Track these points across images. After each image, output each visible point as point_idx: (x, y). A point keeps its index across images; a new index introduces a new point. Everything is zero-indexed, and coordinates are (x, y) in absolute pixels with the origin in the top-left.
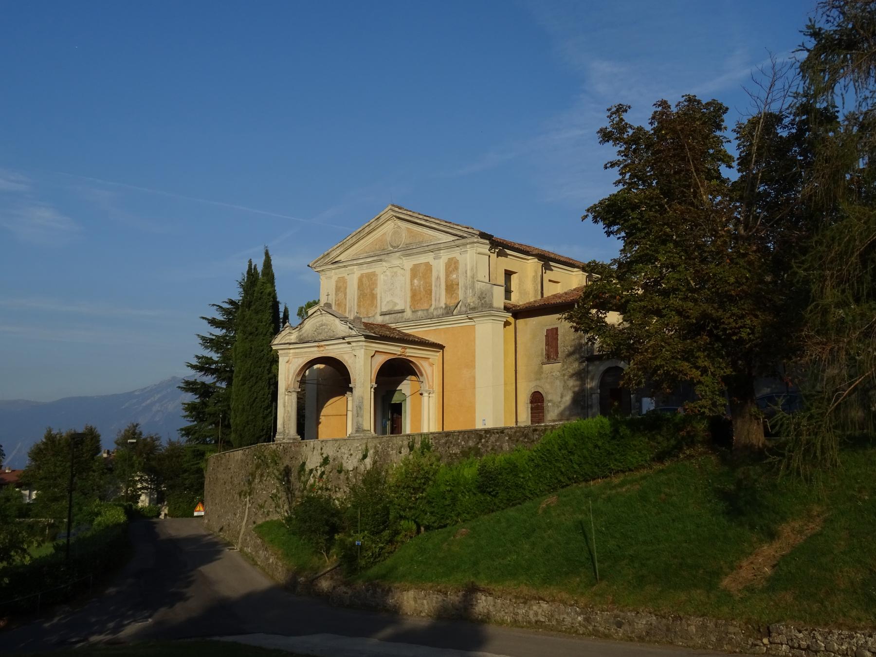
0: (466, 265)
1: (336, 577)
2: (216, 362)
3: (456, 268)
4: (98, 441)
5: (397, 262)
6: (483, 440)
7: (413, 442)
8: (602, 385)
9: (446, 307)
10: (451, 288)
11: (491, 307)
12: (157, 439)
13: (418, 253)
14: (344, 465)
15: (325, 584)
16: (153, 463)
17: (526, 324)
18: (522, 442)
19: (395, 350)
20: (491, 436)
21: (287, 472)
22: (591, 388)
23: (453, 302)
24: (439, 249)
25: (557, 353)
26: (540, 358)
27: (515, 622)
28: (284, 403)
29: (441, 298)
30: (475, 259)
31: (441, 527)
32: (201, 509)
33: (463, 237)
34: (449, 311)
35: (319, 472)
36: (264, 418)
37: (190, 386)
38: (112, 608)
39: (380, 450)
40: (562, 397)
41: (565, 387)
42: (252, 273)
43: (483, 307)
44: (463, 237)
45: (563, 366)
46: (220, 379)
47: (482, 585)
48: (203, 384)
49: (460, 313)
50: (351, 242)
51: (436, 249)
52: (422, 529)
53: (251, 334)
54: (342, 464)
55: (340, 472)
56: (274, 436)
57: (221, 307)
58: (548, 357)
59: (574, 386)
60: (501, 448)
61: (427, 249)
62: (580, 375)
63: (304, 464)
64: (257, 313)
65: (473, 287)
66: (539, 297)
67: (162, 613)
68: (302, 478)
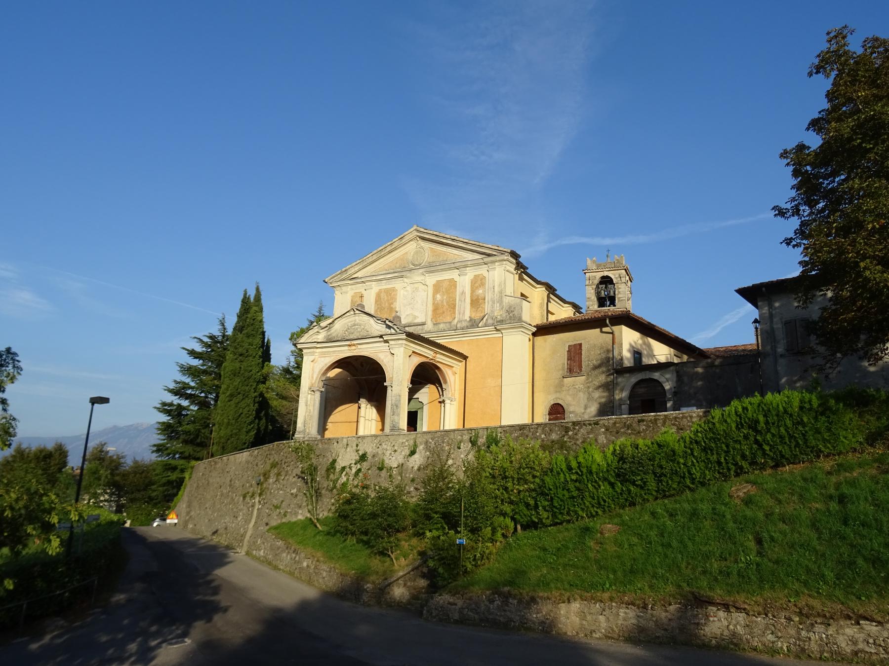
0: (494, 281)
1: (409, 584)
2: (192, 388)
3: (483, 284)
4: (66, 456)
5: (420, 278)
6: (570, 433)
7: (477, 436)
8: (631, 396)
9: (471, 320)
10: (476, 302)
11: (520, 320)
12: (123, 457)
13: (442, 270)
14: (387, 461)
15: (399, 592)
16: (117, 478)
17: (545, 341)
18: (625, 433)
19: (429, 353)
20: (581, 427)
21: (313, 470)
22: (621, 399)
23: (477, 316)
24: (466, 266)
25: (580, 367)
27: (802, 653)
28: (307, 401)
29: (466, 312)
30: (501, 276)
31: (555, 524)
32: (175, 517)
33: (489, 255)
34: (473, 324)
35: (354, 470)
36: (247, 432)
37: (165, 408)
38: (126, 622)
39: (433, 445)
40: (586, 408)
41: (590, 399)
42: (245, 301)
43: (512, 319)
44: (489, 255)
45: (588, 379)
46: (192, 403)
47: (718, 594)
48: (179, 405)
49: (486, 326)
50: (371, 260)
51: (461, 266)
52: (519, 527)
53: (241, 355)
54: (383, 461)
55: (381, 469)
56: (293, 435)
57: (201, 340)
58: (570, 370)
59: (600, 397)
60: (596, 440)
61: (453, 266)
62: (609, 387)
63: (334, 461)
64: (248, 337)
65: (501, 301)
66: (545, 321)
67: (199, 630)
68: (332, 476)
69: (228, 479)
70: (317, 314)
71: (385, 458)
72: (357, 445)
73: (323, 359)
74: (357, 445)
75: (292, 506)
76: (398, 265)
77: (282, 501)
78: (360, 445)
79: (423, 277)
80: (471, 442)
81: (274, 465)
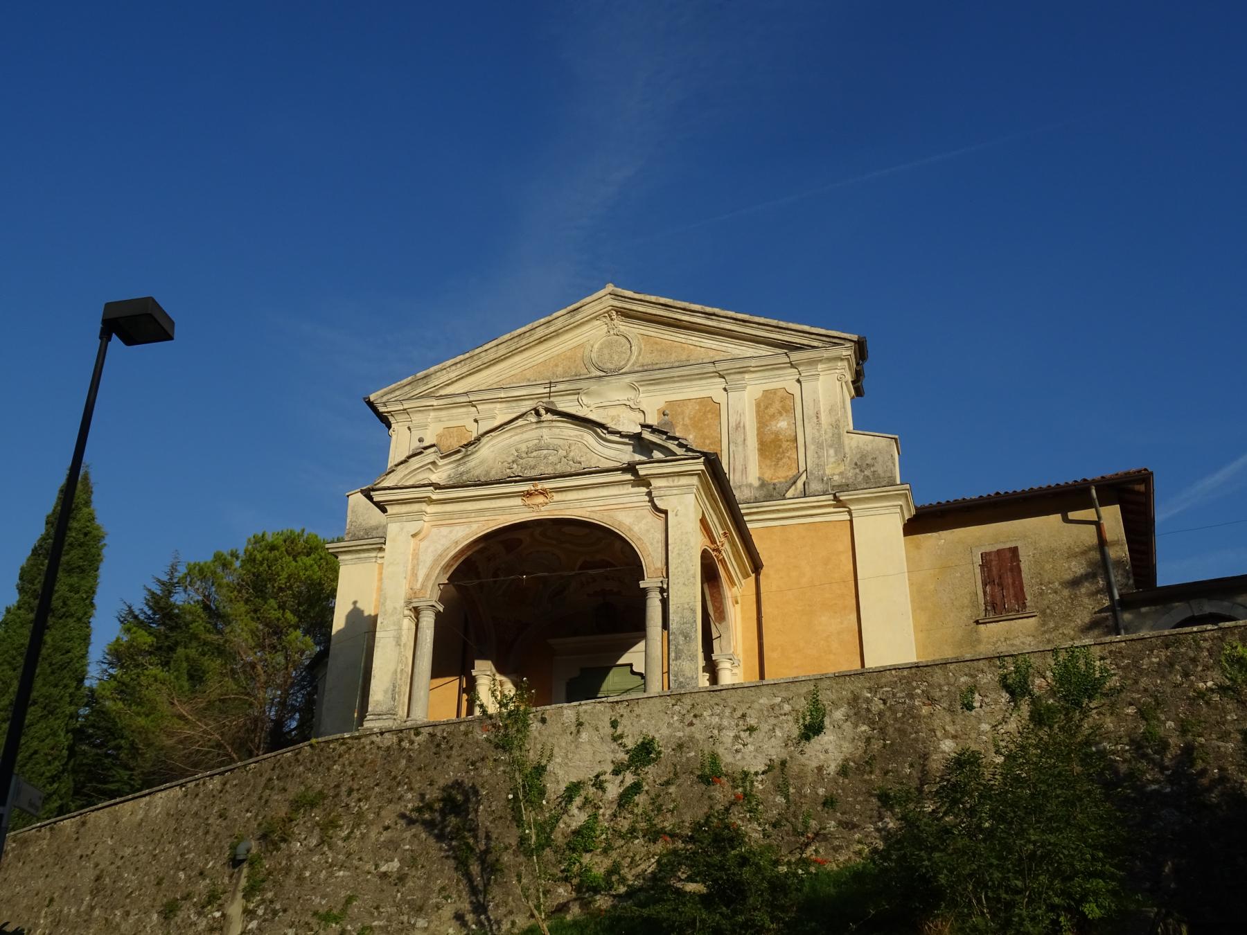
0: (816, 402)
9: (763, 484)
10: (770, 447)
13: (683, 378)
14: (726, 758)
17: (918, 547)
23: (780, 475)
26: (968, 612)
35: (613, 790)
50: (492, 355)
54: (714, 757)
63: (540, 770)
69: (91, 874)
70: (165, 578)
71: (720, 750)
72: (614, 724)
73: (445, 530)
74: (614, 724)
75: (388, 909)
76: (560, 370)
77: (349, 900)
78: (624, 721)
79: (631, 394)
80: (1007, 687)
81: (302, 804)
